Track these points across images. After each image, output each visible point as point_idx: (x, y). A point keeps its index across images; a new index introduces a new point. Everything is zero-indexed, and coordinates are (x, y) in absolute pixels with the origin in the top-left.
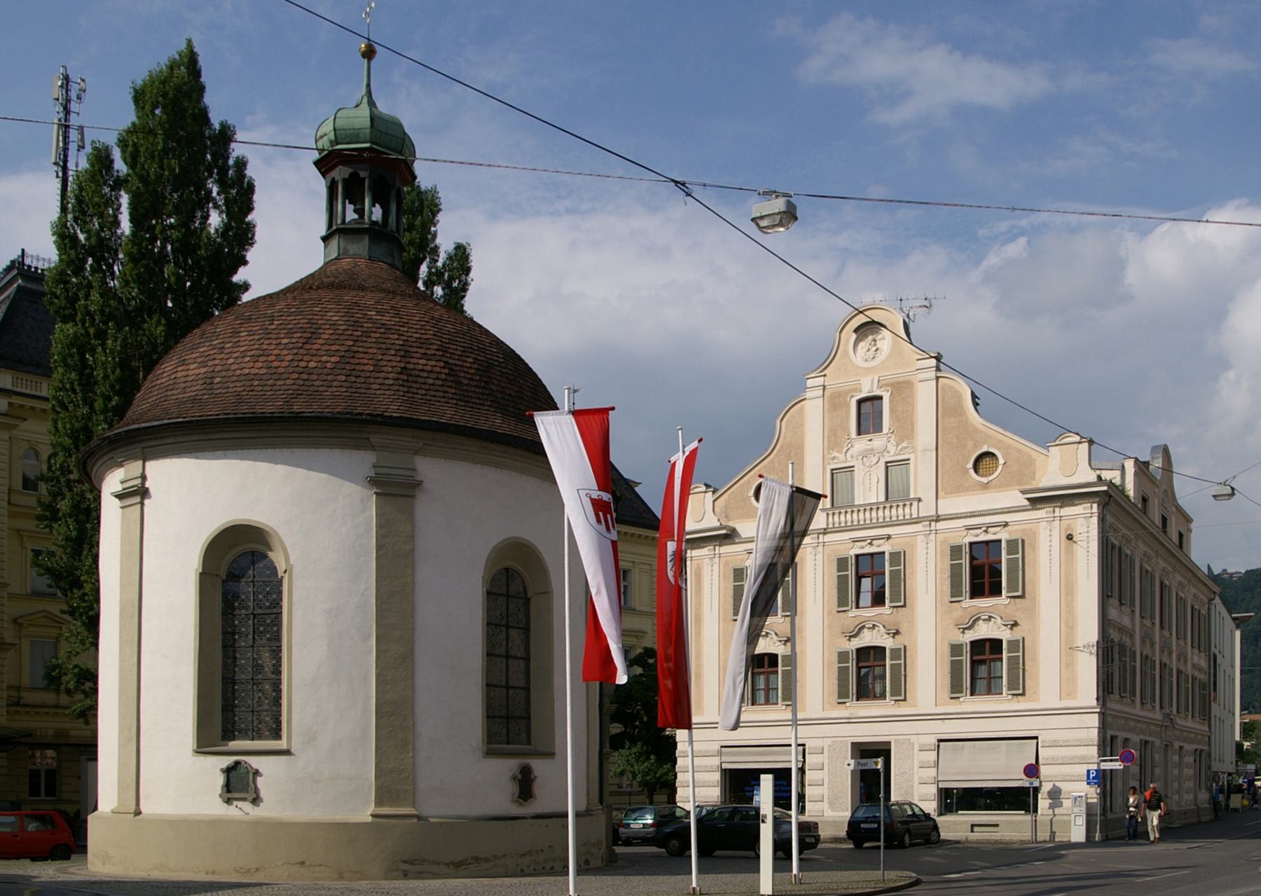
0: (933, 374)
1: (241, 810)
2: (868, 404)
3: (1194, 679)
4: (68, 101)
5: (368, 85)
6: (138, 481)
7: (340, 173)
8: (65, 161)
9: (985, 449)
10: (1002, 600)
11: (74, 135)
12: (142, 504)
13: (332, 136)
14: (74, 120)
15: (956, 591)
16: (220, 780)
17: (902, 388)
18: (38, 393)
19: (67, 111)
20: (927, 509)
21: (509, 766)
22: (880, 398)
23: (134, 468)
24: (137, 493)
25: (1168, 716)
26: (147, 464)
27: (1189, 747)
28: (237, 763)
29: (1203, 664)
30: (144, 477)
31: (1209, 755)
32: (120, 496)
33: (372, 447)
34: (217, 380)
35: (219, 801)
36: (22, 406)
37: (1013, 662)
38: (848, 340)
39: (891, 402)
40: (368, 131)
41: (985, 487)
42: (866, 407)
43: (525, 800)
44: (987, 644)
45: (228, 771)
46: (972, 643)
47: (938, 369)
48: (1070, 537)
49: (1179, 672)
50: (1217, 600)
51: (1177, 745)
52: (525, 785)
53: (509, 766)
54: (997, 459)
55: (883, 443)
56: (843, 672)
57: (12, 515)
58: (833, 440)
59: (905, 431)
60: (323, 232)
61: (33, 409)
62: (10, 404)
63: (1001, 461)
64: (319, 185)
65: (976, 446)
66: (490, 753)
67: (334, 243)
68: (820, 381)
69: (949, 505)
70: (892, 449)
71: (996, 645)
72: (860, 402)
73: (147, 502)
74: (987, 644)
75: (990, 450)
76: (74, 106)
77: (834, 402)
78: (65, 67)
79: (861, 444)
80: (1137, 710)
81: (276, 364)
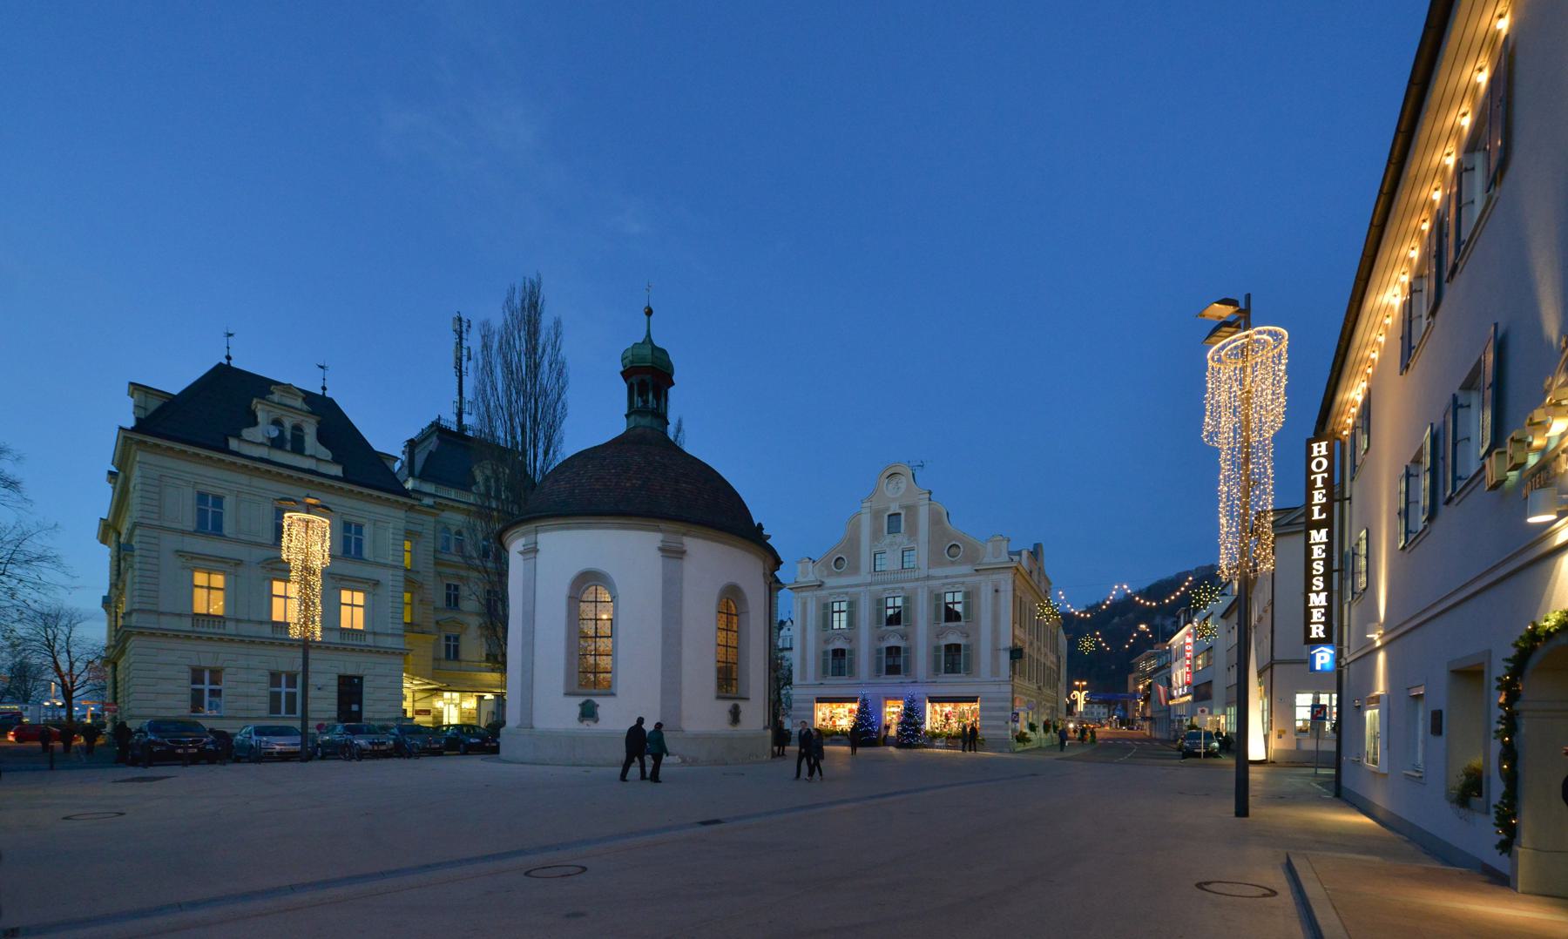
0: (927, 502)
1: (589, 727)
2: (894, 517)
3: (1051, 668)
4: (461, 332)
5: (649, 331)
6: (533, 546)
7: (633, 380)
8: (461, 367)
9: (954, 543)
10: (901, 627)
11: (465, 352)
12: (535, 558)
13: (631, 358)
14: (465, 344)
15: (937, 618)
16: (578, 710)
17: (911, 509)
18: (449, 497)
19: (461, 338)
20: (923, 572)
21: (728, 704)
22: (900, 514)
23: (532, 538)
24: (531, 551)
25: (1039, 688)
26: (539, 535)
27: (1048, 705)
28: (588, 701)
29: (1055, 660)
30: (536, 543)
31: (1057, 710)
32: (521, 553)
33: (660, 531)
34: (577, 491)
35: (577, 721)
36: (441, 504)
37: (967, 656)
38: (883, 482)
39: (906, 516)
40: (650, 357)
41: (953, 563)
42: (893, 518)
43: (736, 723)
44: (894, 649)
45: (583, 705)
46: (833, 650)
47: (930, 500)
48: (997, 591)
49: (1037, 660)
50: (1061, 628)
51: (1043, 703)
52: (735, 716)
53: (728, 704)
54: (959, 547)
55: (901, 539)
56: (879, 660)
57: (436, 564)
58: (876, 535)
59: (913, 531)
60: (626, 412)
61: (446, 505)
62: (435, 502)
63: (962, 549)
64: (624, 387)
65: (949, 542)
66: (718, 697)
67: (632, 418)
68: (869, 504)
69: (933, 572)
70: (905, 541)
71: (958, 647)
72: (889, 516)
73: (538, 556)
74: (894, 649)
75: (957, 543)
76: (464, 336)
77: (876, 515)
78: (459, 312)
79: (888, 539)
80: (1027, 684)
81: (609, 484)
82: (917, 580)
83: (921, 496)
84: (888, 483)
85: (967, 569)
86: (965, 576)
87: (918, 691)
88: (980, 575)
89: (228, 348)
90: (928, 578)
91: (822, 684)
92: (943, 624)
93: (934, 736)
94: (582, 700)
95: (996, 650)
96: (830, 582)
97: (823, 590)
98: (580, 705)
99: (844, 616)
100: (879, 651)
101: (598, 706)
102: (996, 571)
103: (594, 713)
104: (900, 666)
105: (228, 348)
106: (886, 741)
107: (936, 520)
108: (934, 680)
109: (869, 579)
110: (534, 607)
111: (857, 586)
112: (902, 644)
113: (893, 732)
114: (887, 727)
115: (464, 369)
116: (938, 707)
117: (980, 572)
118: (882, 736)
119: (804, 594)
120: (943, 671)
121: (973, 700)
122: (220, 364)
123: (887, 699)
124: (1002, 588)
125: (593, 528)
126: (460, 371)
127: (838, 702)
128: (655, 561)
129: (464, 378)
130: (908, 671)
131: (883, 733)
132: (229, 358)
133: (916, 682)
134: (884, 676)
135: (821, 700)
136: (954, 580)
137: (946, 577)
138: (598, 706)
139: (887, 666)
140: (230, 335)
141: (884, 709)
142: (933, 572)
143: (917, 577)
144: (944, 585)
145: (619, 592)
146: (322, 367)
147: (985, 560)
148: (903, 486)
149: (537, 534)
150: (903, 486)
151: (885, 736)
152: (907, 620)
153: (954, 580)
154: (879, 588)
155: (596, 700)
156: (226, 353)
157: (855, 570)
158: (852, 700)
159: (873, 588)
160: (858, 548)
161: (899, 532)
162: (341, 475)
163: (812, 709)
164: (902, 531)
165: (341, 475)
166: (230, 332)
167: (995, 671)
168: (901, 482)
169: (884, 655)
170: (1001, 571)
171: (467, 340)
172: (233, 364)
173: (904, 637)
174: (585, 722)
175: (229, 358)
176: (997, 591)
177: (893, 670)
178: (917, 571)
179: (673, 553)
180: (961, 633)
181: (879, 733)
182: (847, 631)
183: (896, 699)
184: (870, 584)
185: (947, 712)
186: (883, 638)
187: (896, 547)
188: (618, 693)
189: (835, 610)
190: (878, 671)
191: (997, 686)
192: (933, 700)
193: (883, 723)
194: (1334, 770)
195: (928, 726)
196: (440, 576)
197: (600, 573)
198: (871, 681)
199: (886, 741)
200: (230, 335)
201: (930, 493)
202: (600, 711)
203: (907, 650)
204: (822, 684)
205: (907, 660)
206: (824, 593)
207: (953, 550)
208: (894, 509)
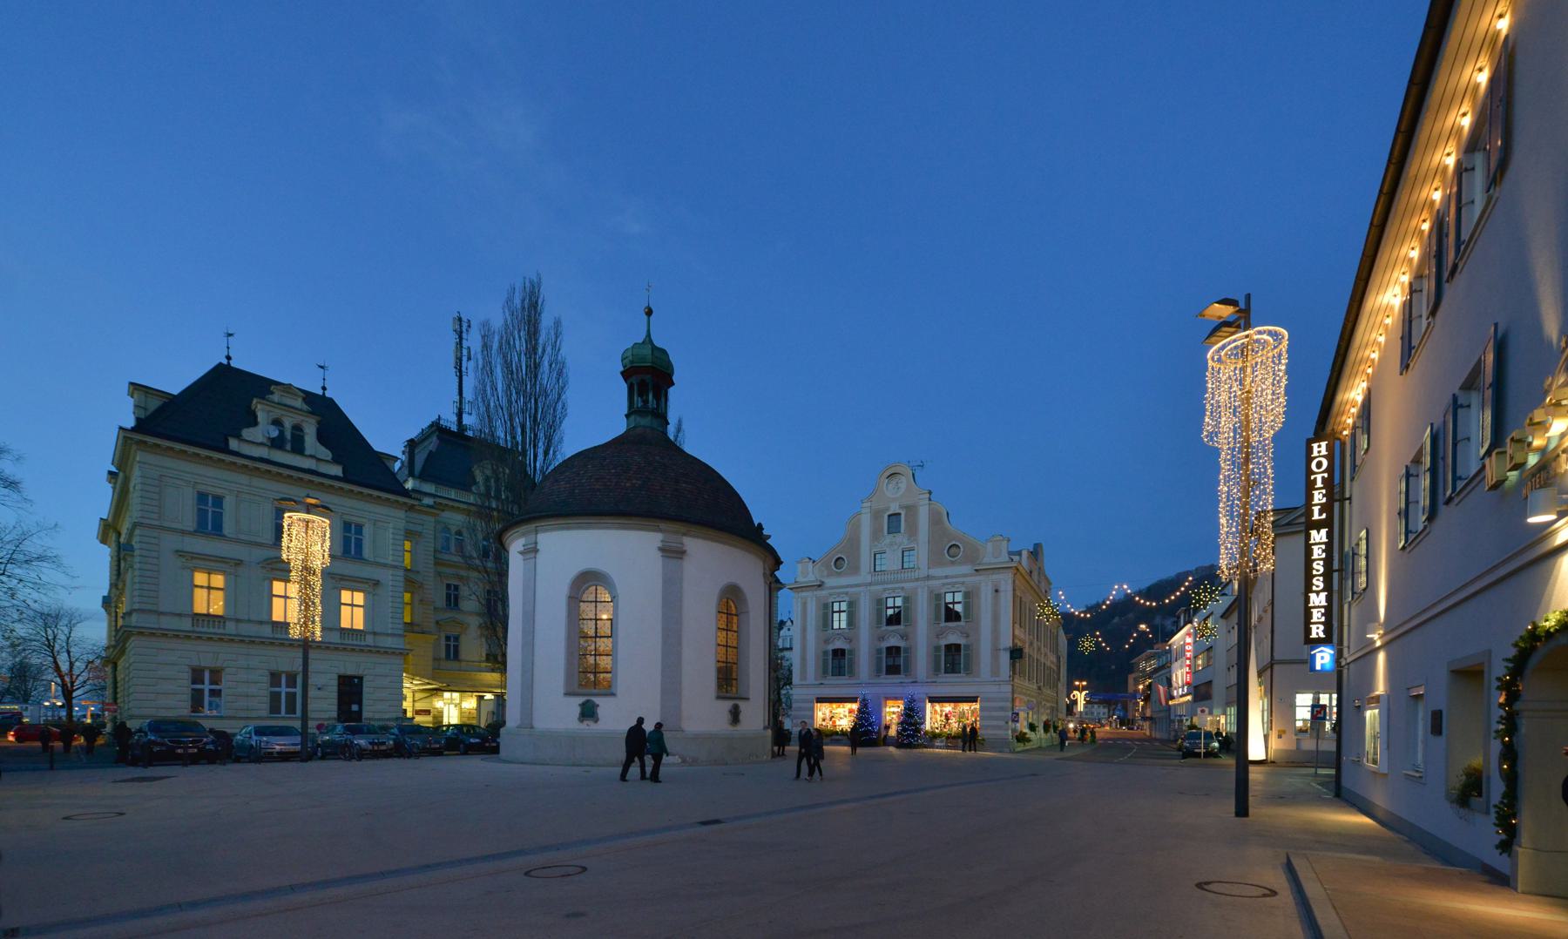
0: (927, 502)
1: (589, 727)
2: (894, 517)
3: (1051, 668)
4: (461, 332)
5: (649, 331)
6: (533, 546)
7: (633, 380)
8: (461, 367)
9: (954, 543)
10: (901, 627)
11: (465, 352)
12: (535, 558)
13: (631, 358)
14: (465, 344)
15: (937, 618)
16: (578, 710)
17: (911, 509)
18: (449, 497)
19: (461, 338)
20: (923, 572)
21: (728, 704)
22: (900, 514)
23: (532, 538)
24: (531, 551)
25: (1039, 688)
26: (539, 535)
27: (1048, 705)
28: (588, 701)
29: (1055, 660)
30: (536, 543)
31: (1057, 710)
32: (521, 553)
33: (660, 531)
34: (577, 491)
35: (577, 721)
36: (441, 504)
37: (967, 656)
38: (883, 482)
39: (906, 516)
40: (650, 357)
41: (953, 563)
42: (893, 518)
43: (736, 723)
44: (894, 649)
45: (583, 705)
46: (833, 650)
47: (930, 500)
48: (997, 591)
49: (1037, 660)
50: (1061, 628)
51: (1043, 703)
52: (735, 716)
53: (728, 704)
54: (959, 547)
55: (901, 539)
56: (879, 660)
57: (436, 564)
58: (876, 535)
59: (913, 531)
60: (626, 412)
61: (446, 505)
62: (435, 502)
63: (962, 549)
64: (624, 387)
65: (949, 542)
66: (718, 697)
67: (632, 418)
68: (869, 504)
69: (933, 572)
70: (905, 541)
71: (958, 647)
72: (889, 516)
73: (538, 556)
74: (894, 649)
75: (957, 543)
76: (464, 336)
77: (876, 515)
78: (459, 312)
79: (888, 539)
80: (1027, 684)
81: (609, 484)
82: (917, 580)
83: (921, 496)
84: (888, 483)
85: (967, 569)
86: (965, 576)
87: (918, 691)
88: (980, 575)
89: (228, 348)
90: (928, 578)
91: (822, 684)
92: (943, 624)
93: (934, 736)
94: (582, 700)
95: (996, 650)
96: (830, 582)
97: (823, 590)
98: (580, 705)
99: (844, 616)
100: (879, 651)
101: (598, 706)
102: (996, 571)
103: (594, 713)
104: (900, 666)
105: (228, 348)
106: (886, 741)
107: (936, 520)
108: (934, 680)
109: (869, 579)
110: (534, 607)
111: (857, 586)
112: (902, 644)
113: (893, 732)
114: (887, 727)
115: (464, 369)
116: (938, 707)
117: (980, 572)
118: (882, 736)
119: (804, 594)
120: (943, 671)
121: (973, 700)
122: (220, 364)
123: (887, 699)
124: (1002, 588)
125: (593, 528)
126: (460, 371)
127: (838, 702)
128: (655, 561)
129: (464, 378)
130: (908, 671)
131: (883, 733)
132: (229, 358)
133: (916, 682)
134: (884, 676)
135: (821, 700)
136: (954, 580)
137: (946, 577)
138: (598, 706)
139: (887, 666)
140: (230, 335)
141: (884, 709)
142: (933, 572)
143: (917, 577)
144: (944, 585)
145: (619, 592)
146: (322, 367)
147: (985, 560)
148: (903, 486)
149: (537, 534)
150: (903, 486)
151: (885, 736)
152: (907, 620)
153: (954, 580)
154: (879, 588)
155: (596, 700)
156: (226, 353)
157: (855, 570)
158: (852, 700)
159: (873, 588)
160: (858, 548)
161: (899, 532)
162: (341, 475)
163: (812, 709)
164: (902, 531)
165: (341, 475)
166: (230, 332)
167: (995, 671)
168: (901, 482)
169: (884, 655)
170: (1001, 571)
171: (467, 340)
172: (233, 364)
173: (904, 637)
174: (585, 722)
175: (229, 358)
176: (997, 591)
177: (893, 670)
178: (917, 571)
179: (673, 553)
180: (961, 633)
181: (879, 733)
182: (847, 631)
183: (896, 699)
184: (870, 584)
185: (947, 712)
186: (883, 638)
187: (896, 547)
188: (618, 693)
189: (835, 610)
190: (878, 671)
191: (997, 686)
192: (933, 700)
193: (883, 723)
194: (1334, 770)
195: (928, 726)
196: (440, 576)
197: (600, 573)
198: (871, 681)
199: (886, 741)
200: (230, 335)
201: (930, 493)
202: (600, 711)
203: (907, 650)
204: (822, 684)
205: (907, 660)
206: (824, 593)
207: (953, 550)
208: (894, 509)
